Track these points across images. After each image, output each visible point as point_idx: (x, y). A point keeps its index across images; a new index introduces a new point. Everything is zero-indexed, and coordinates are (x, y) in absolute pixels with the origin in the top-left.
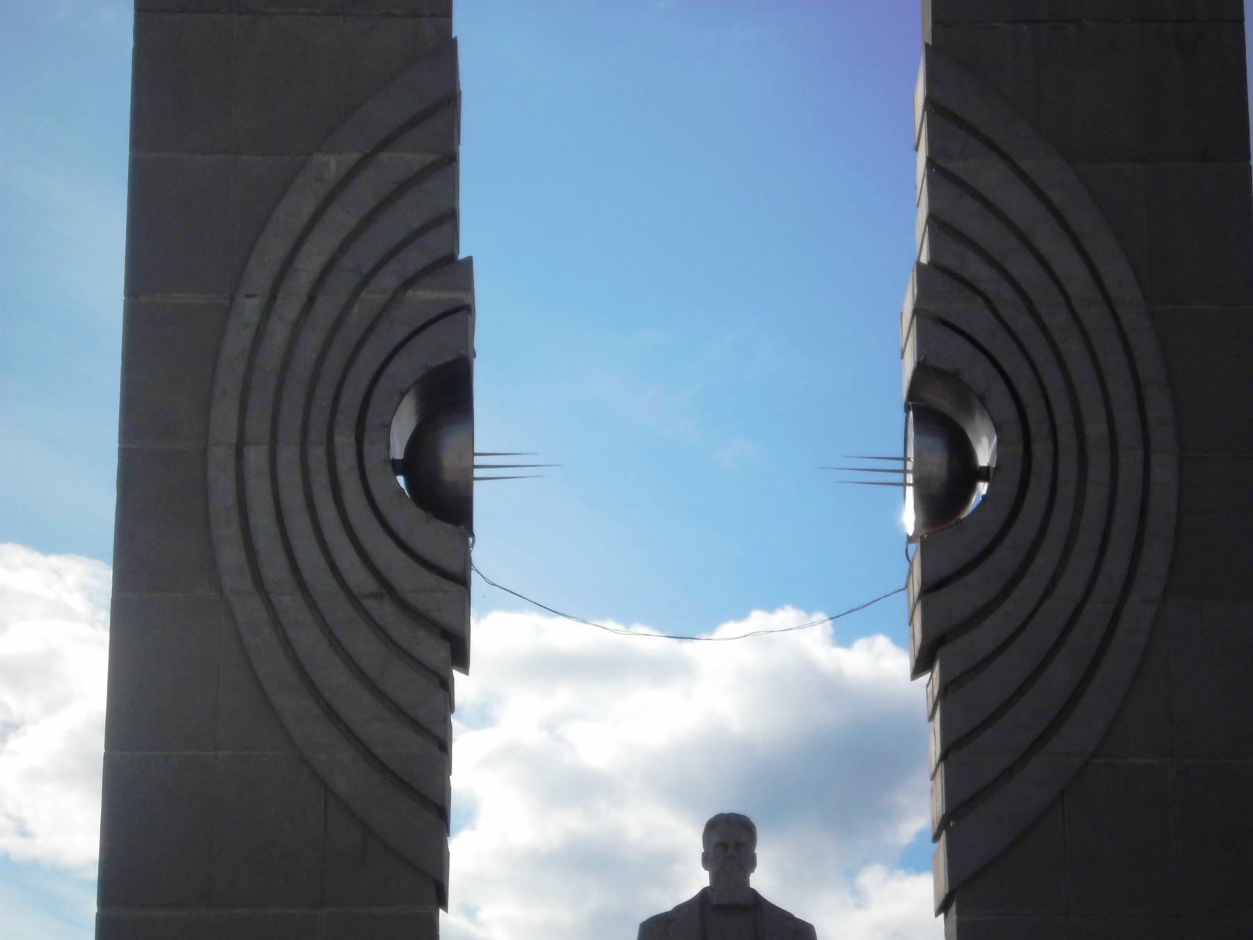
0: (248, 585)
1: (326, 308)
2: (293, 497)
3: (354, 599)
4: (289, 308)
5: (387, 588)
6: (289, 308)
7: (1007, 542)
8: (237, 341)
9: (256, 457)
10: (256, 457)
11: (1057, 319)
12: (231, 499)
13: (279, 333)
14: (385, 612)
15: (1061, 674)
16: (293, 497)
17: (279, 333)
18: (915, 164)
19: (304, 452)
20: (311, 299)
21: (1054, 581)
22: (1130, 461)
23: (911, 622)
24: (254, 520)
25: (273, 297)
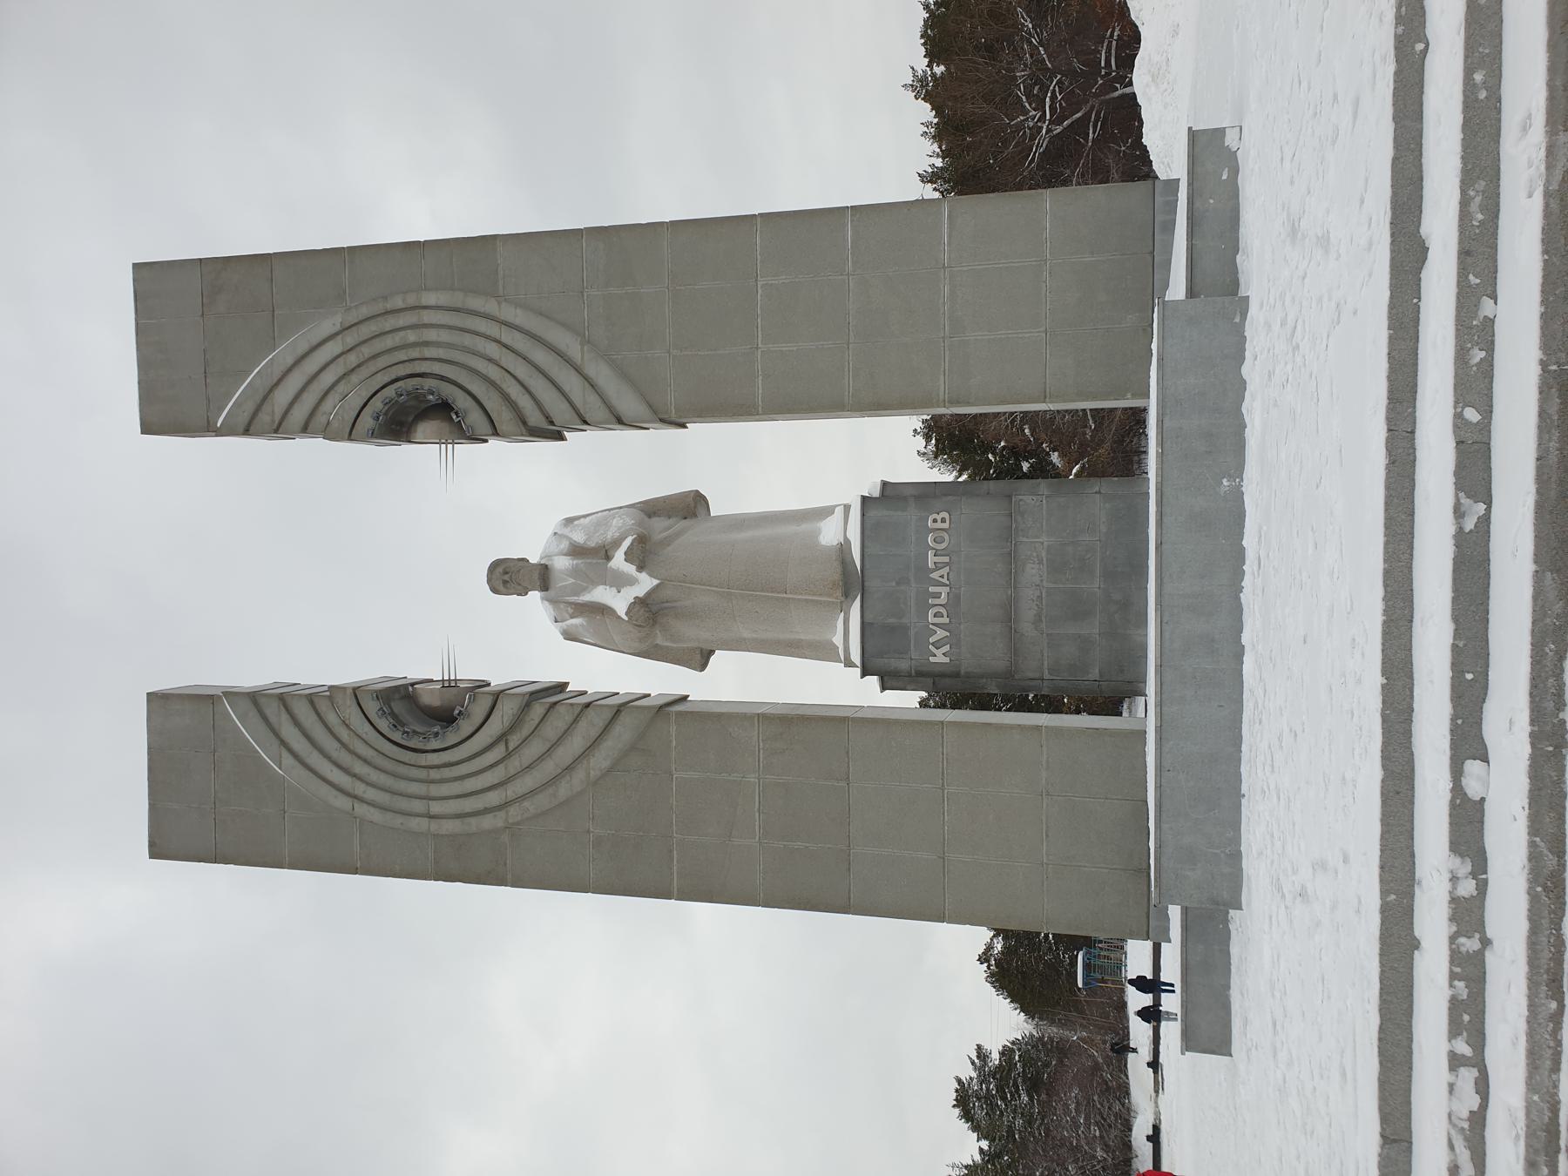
0: (502, 814)
1: (360, 768)
2: (456, 788)
3: (509, 755)
4: (360, 789)
5: (502, 737)
6: (360, 789)
7: (469, 387)
8: (375, 815)
9: (436, 808)
10: (436, 808)
11: (352, 359)
12: (458, 822)
13: (371, 794)
14: (514, 740)
15: (541, 356)
16: (456, 788)
17: (371, 794)
18: (620, 709)
19: (433, 782)
20: (354, 775)
21: (490, 360)
22: (432, 335)
23: (1155, 1138)
24: (468, 810)
25: (355, 797)
